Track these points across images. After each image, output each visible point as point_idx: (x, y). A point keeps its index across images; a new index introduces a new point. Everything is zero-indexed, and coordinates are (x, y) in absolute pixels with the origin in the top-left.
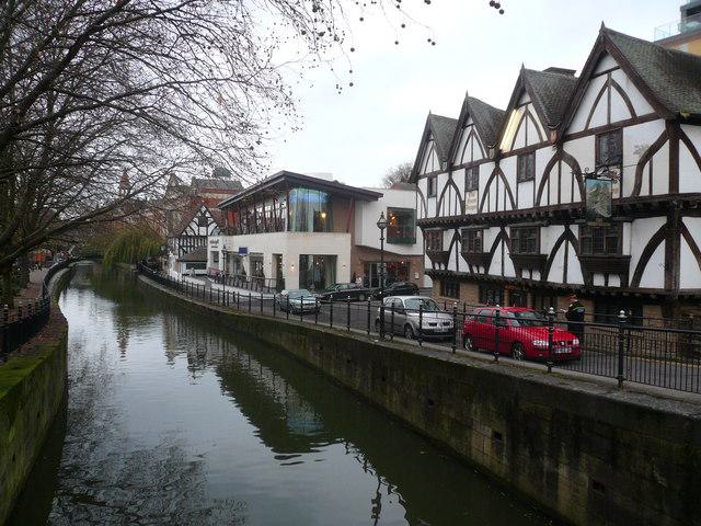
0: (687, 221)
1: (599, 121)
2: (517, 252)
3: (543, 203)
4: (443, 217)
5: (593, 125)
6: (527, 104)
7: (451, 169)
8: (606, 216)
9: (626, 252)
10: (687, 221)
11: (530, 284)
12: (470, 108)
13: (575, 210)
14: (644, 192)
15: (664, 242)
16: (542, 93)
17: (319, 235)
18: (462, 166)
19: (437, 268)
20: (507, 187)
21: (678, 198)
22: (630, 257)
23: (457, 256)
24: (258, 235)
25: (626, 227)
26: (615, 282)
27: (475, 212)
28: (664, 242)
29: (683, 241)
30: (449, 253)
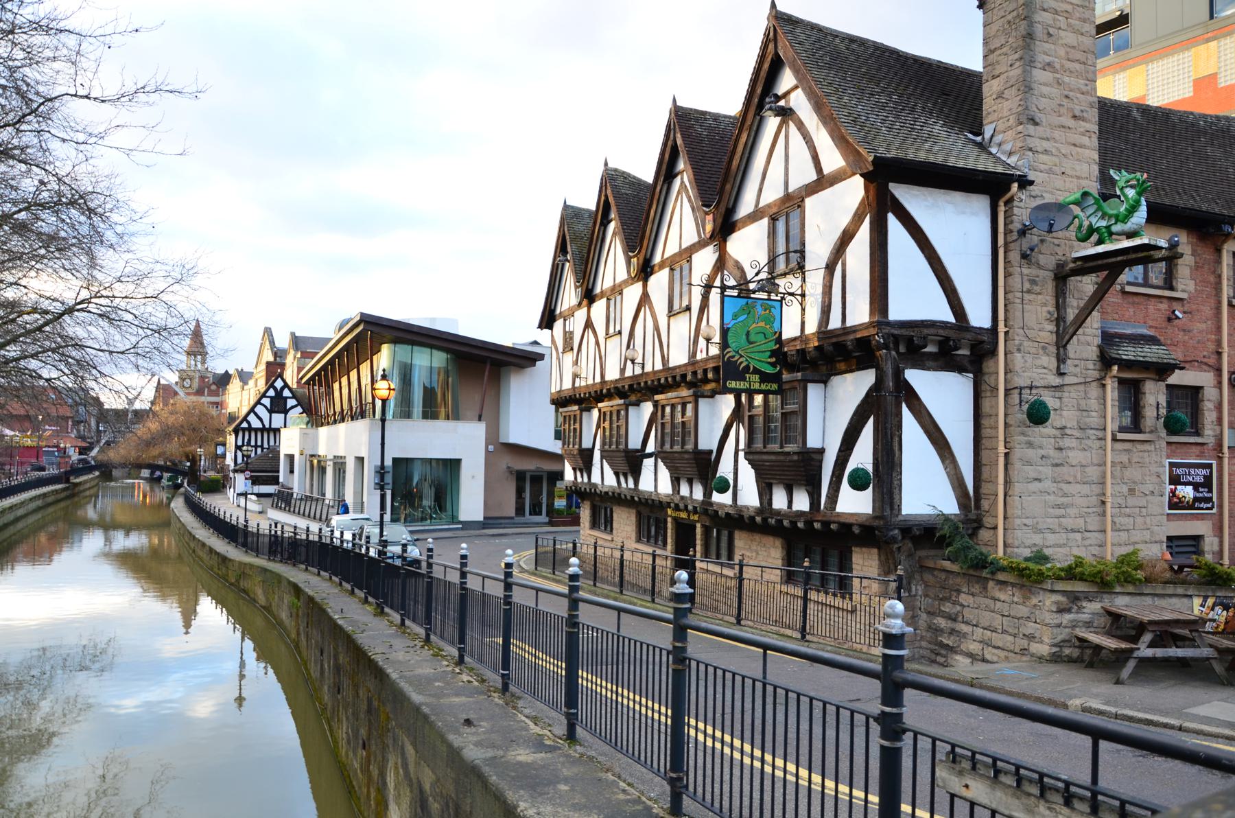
0: (915, 377)
1: (772, 194)
3: (700, 356)
4: (845, 331)
7: (645, 271)
8: (769, 370)
9: (813, 442)
10: (915, 377)
11: (650, 502)
12: (614, 182)
13: (631, 386)
17: (430, 423)
18: (754, 217)
19: (579, 480)
20: (657, 328)
21: (887, 330)
22: (821, 451)
23: (736, 461)
24: (1221, 114)
26: (802, 502)
27: (617, 376)
29: (907, 416)
30: (591, 451)
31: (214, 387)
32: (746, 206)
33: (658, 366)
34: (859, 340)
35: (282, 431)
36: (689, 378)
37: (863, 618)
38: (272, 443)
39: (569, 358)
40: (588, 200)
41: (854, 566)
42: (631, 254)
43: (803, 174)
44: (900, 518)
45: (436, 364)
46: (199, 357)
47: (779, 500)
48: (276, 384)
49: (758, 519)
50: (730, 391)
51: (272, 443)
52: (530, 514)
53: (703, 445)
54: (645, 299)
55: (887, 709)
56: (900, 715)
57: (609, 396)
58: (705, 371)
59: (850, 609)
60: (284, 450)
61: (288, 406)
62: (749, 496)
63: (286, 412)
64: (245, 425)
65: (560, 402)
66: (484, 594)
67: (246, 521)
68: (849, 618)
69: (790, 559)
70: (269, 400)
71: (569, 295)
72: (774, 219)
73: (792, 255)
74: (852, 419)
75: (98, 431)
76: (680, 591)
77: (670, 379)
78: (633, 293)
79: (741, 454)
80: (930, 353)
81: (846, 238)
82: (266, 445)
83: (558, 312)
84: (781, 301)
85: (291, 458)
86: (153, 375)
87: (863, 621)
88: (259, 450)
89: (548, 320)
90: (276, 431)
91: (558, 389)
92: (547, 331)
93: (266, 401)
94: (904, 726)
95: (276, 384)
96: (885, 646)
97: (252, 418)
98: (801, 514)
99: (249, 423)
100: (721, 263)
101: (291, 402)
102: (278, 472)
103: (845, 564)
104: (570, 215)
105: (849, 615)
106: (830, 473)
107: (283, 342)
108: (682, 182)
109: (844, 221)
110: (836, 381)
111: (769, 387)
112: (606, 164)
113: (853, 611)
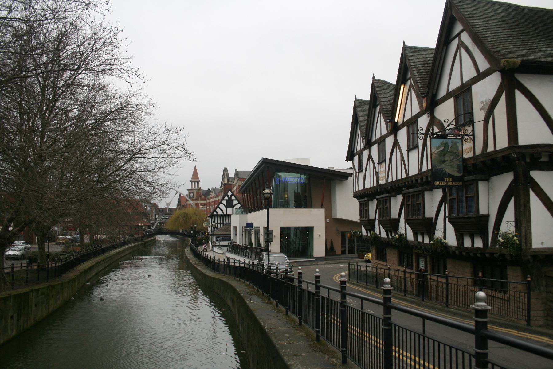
0: (536, 175)
1: (455, 84)
2: (410, 218)
4: (496, 152)
5: (453, 87)
6: (459, 35)
8: (457, 174)
9: (483, 211)
10: (536, 175)
14: (490, 148)
15: (531, 190)
16: (420, 65)
20: (402, 157)
22: (487, 217)
25: (482, 187)
26: (479, 243)
28: (531, 190)
29: (533, 196)
31: (203, 197)
32: (442, 92)
33: (404, 176)
34: (503, 157)
35: (232, 216)
36: (419, 181)
37: (513, 304)
38: (227, 222)
39: (361, 176)
40: (366, 96)
41: (508, 276)
42: (388, 121)
43: (469, 73)
44: (531, 250)
45: (300, 181)
46: (196, 183)
47: (467, 243)
48: (228, 194)
49: (457, 252)
50: (438, 187)
51: (227, 222)
52: (349, 253)
53: (427, 215)
54: (396, 144)
55: (478, 351)
56: (486, 355)
57: (381, 193)
58: (427, 177)
59: (506, 299)
60: (233, 225)
61: (234, 204)
62: (451, 240)
63: (233, 206)
64: (215, 213)
65: (357, 195)
66: (308, 292)
67: (214, 258)
68: (506, 304)
69: (475, 274)
70: (225, 201)
71: (360, 144)
72: (456, 98)
73: (466, 115)
74: (503, 198)
75: (156, 219)
76: (386, 288)
77: (410, 182)
78: (389, 141)
79: (447, 219)
80: (544, 162)
81: (494, 103)
82: (225, 223)
83: (355, 152)
84: (462, 139)
85: (236, 228)
86: (177, 192)
87: (513, 305)
88: (222, 225)
89: (350, 157)
90: (229, 216)
91: (357, 190)
92: (351, 162)
93: (224, 202)
94: (488, 360)
95: (228, 194)
96: (476, 316)
97: (218, 210)
98: (478, 249)
99: (217, 212)
100: (433, 121)
101: (235, 202)
102: (231, 235)
103: (504, 276)
104: (358, 103)
105: (506, 302)
106: (492, 227)
107: (232, 174)
108: (411, 83)
109: (491, 95)
110: (494, 179)
111: (457, 184)
112: (374, 77)
113: (508, 300)
